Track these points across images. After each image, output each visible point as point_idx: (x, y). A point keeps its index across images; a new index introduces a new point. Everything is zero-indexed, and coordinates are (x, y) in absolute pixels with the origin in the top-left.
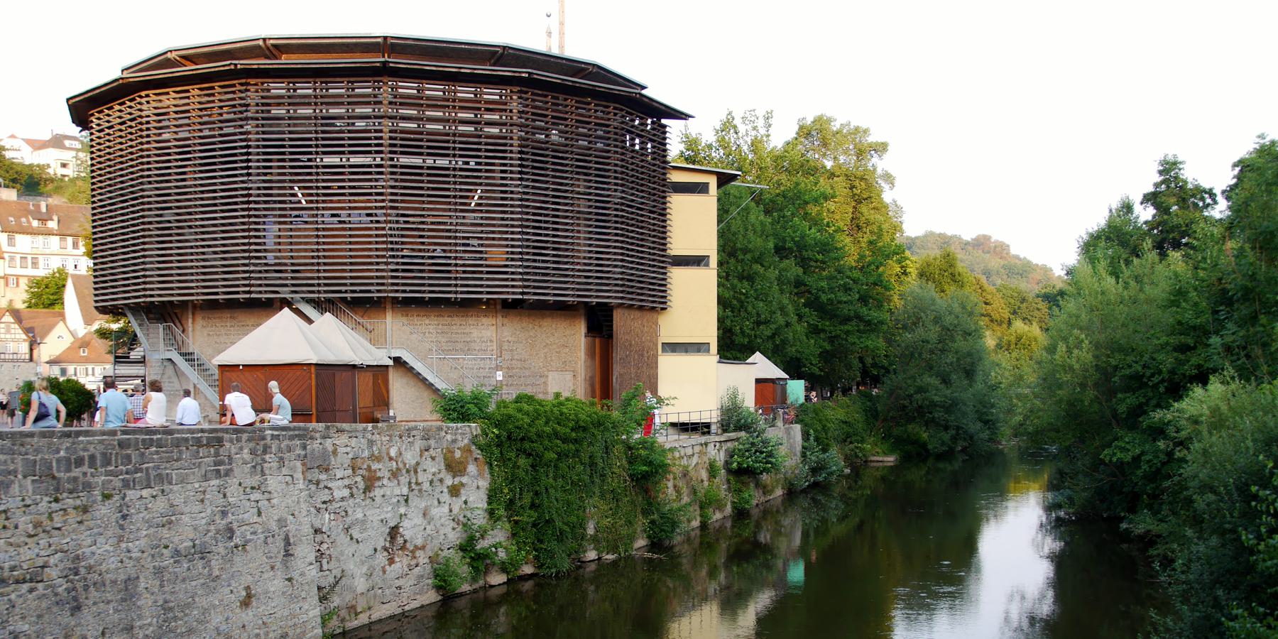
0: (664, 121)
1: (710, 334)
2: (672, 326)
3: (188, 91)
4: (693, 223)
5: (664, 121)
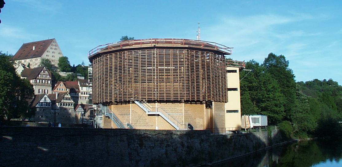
0: (225, 55)
1: (238, 107)
2: (228, 106)
3: (198, 52)
4: (233, 80)
5: (225, 55)
